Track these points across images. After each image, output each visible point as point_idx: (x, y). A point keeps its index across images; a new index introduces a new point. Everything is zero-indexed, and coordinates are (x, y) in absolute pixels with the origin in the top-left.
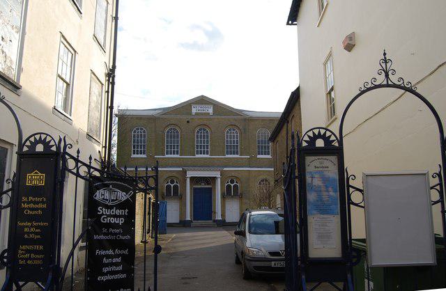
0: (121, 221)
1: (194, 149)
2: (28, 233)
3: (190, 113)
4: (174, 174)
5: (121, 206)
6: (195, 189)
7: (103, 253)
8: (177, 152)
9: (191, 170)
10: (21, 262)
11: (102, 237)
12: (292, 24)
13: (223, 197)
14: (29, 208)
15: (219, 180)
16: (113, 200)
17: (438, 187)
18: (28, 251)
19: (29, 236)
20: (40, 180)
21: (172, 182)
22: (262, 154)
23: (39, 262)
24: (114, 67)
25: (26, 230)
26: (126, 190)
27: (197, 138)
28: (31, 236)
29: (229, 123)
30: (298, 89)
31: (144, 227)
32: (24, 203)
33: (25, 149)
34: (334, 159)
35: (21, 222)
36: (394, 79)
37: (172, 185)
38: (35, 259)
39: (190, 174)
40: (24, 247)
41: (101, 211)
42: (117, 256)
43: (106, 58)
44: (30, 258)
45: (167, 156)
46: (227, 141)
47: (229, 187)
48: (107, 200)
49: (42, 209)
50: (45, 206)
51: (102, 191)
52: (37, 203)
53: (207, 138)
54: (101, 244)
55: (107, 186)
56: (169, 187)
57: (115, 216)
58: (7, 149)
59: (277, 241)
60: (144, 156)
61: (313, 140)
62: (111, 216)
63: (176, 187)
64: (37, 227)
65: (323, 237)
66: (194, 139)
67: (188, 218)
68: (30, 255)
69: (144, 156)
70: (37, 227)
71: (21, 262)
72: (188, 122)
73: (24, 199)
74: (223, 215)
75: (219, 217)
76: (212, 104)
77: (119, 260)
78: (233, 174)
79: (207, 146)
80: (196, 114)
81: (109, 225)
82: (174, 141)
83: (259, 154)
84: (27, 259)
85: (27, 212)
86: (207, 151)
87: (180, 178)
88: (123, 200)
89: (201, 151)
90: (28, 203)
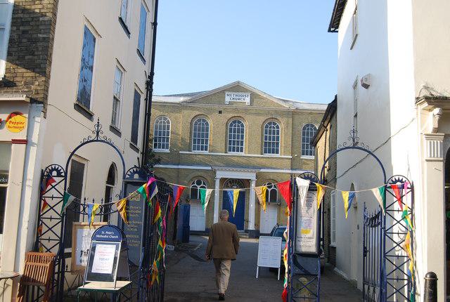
3: (222, 102)
12: (334, 31)
24: (152, 74)
30: (335, 101)
33: (127, 176)
36: (359, 145)
39: (220, 174)
43: (147, 68)
45: (193, 152)
58: (84, 165)
60: (167, 151)
80: (230, 103)
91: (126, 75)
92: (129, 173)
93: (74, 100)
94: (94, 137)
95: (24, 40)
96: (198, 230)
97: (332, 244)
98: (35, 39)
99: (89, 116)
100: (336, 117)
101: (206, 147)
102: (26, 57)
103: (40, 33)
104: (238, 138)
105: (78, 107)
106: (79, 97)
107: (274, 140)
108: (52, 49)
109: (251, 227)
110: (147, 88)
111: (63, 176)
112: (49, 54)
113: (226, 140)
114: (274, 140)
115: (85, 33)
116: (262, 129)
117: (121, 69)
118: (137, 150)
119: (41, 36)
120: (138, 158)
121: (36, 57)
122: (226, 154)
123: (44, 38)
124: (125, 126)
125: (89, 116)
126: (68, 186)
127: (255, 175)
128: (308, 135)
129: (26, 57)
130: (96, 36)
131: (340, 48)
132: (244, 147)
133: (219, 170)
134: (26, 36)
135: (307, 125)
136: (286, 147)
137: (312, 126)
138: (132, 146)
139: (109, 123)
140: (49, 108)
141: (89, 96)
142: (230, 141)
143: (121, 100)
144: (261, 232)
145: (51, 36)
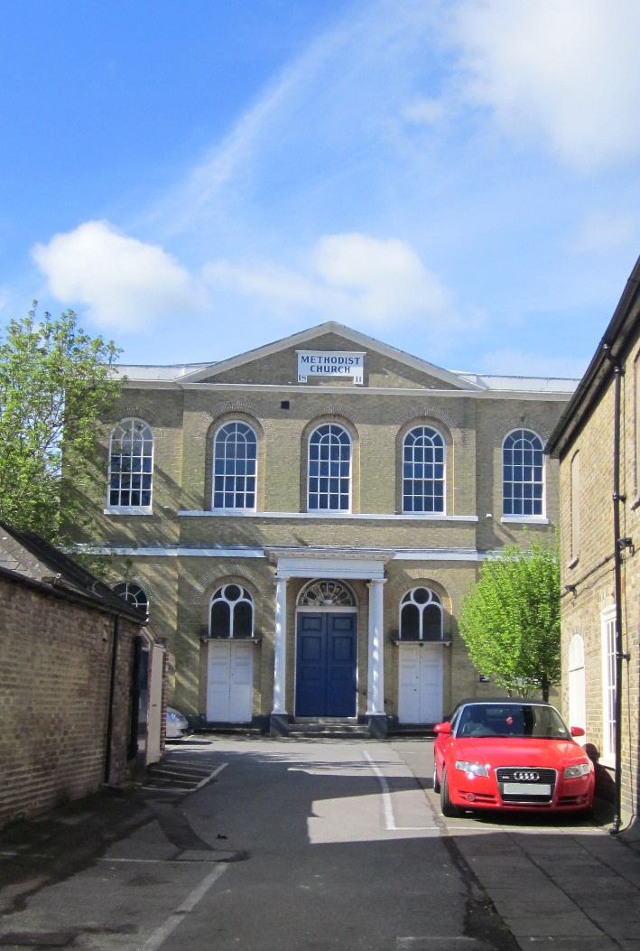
9: (287, 557)
13: (391, 639)
15: (380, 589)
21: (233, 593)
31: (421, 552)
47: (410, 613)
56: (220, 610)
59: (86, 682)
67: (279, 707)
76: (354, 347)
89: (324, 498)
96: (417, 722)
97: (317, 806)
101: (345, 500)
109: (375, 708)
113: (303, 479)
116: (303, 447)
122: (207, 514)
127: (380, 566)
132: (350, 494)
133: (285, 557)
136: (461, 492)
142: (313, 482)
144: (214, 715)
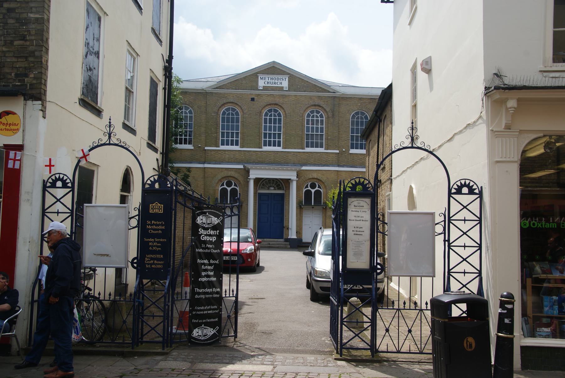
0: (214, 239)
1: (260, 138)
2: (152, 246)
4: (232, 174)
5: (215, 228)
6: (260, 195)
7: (202, 262)
8: (237, 141)
9: (256, 169)
10: (147, 266)
11: (201, 250)
13: (300, 206)
14: (152, 229)
16: (208, 224)
17: (443, 223)
18: (152, 259)
19: (152, 248)
20: (160, 209)
21: (229, 184)
22: (357, 148)
23: (160, 266)
24: (171, 57)
25: (150, 244)
26: (217, 216)
27: (265, 122)
28: (154, 248)
29: (312, 103)
30: (391, 86)
32: (149, 225)
33: (147, 186)
34: (368, 200)
35: (147, 238)
36: (418, 144)
37: (229, 189)
38: (157, 264)
39: (254, 174)
40: (149, 256)
41: (201, 231)
42: (210, 265)
43: (164, 50)
44: (154, 264)
45: (222, 148)
46: (308, 128)
47: (308, 193)
48: (204, 223)
49: (161, 230)
50: (164, 227)
51: (201, 217)
52: (156, 225)
53: (280, 123)
54: (201, 256)
55: (205, 213)
56: (224, 191)
57: (210, 235)
60: (190, 147)
61: (354, 187)
62: (207, 235)
63: (234, 192)
64: (158, 242)
65: (358, 254)
66: (260, 124)
68: (154, 262)
69: (190, 147)
70: (158, 242)
71: (147, 266)
72: (253, 99)
73: (149, 222)
74: (299, 232)
75: (293, 235)
77: (212, 268)
78: (315, 175)
79: (279, 135)
80: (265, 88)
81: (205, 242)
82: (233, 126)
83: (352, 148)
84: (151, 264)
85: (151, 231)
86: (279, 142)
87: (241, 179)
88: (216, 223)
89: (270, 142)
90: (152, 225)
91: (139, 60)
92: (149, 182)
93: (78, 94)
94: (105, 139)
95: (11, 21)
98: (25, 19)
99: (98, 112)
100: (391, 106)
102: (16, 43)
103: (31, 13)
104: (275, 130)
105: (84, 103)
106: (85, 91)
107: (317, 131)
108: (48, 32)
110: (165, 75)
111: (69, 187)
112: (45, 39)
114: (317, 131)
115: (88, 11)
117: (134, 54)
118: (155, 150)
119: (32, 15)
120: (157, 160)
121: (28, 43)
123: (37, 19)
124: (142, 127)
125: (98, 112)
126: (75, 200)
128: (357, 125)
129: (16, 43)
130: (101, 14)
131: (508, 300)
133: (253, 169)
134: (13, 15)
135: (357, 113)
137: (363, 114)
138: (150, 146)
139: (122, 119)
140: (49, 106)
141: (97, 88)
143: (134, 91)
145: (46, 17)
